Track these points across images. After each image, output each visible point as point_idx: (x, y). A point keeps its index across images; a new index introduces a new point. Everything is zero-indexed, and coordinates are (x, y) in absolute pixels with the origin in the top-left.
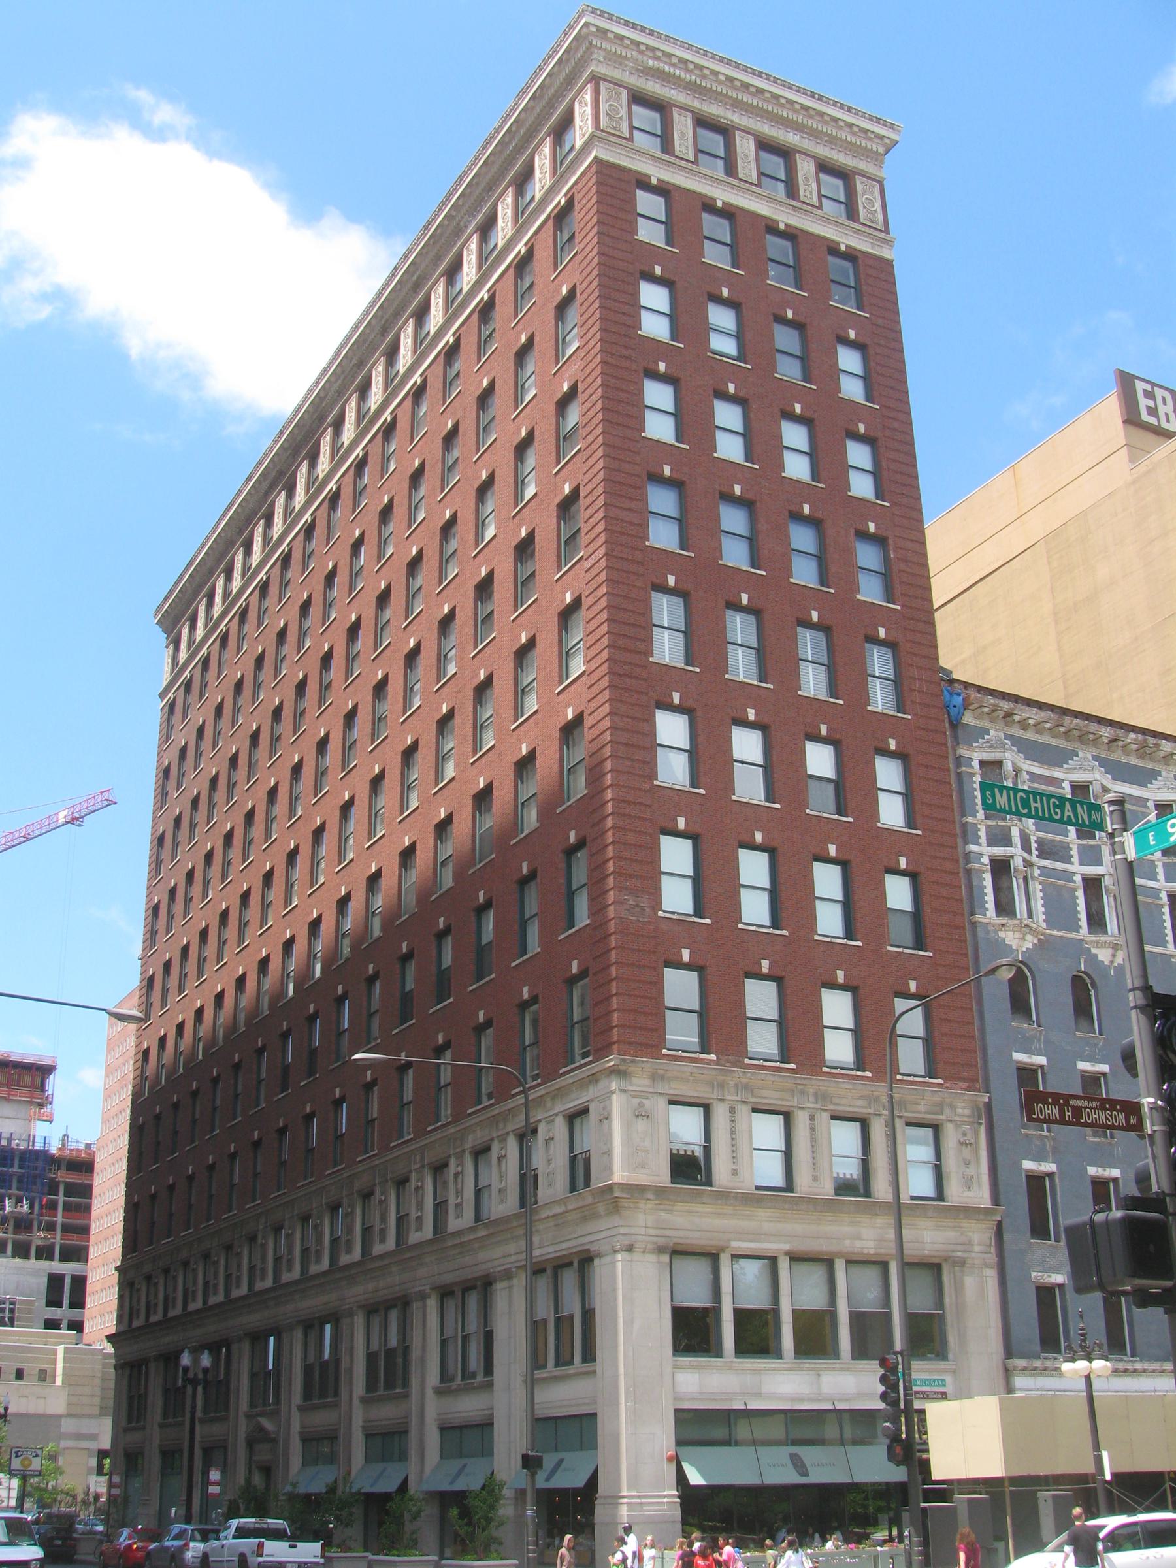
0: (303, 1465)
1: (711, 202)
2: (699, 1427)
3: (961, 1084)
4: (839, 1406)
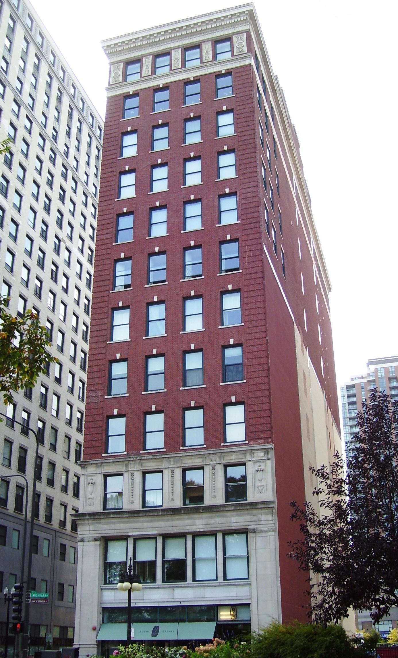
0: (103, 622)
1: (158, 87)
2: (110, 614)
3: (259, 441)
4: (183, 604)
